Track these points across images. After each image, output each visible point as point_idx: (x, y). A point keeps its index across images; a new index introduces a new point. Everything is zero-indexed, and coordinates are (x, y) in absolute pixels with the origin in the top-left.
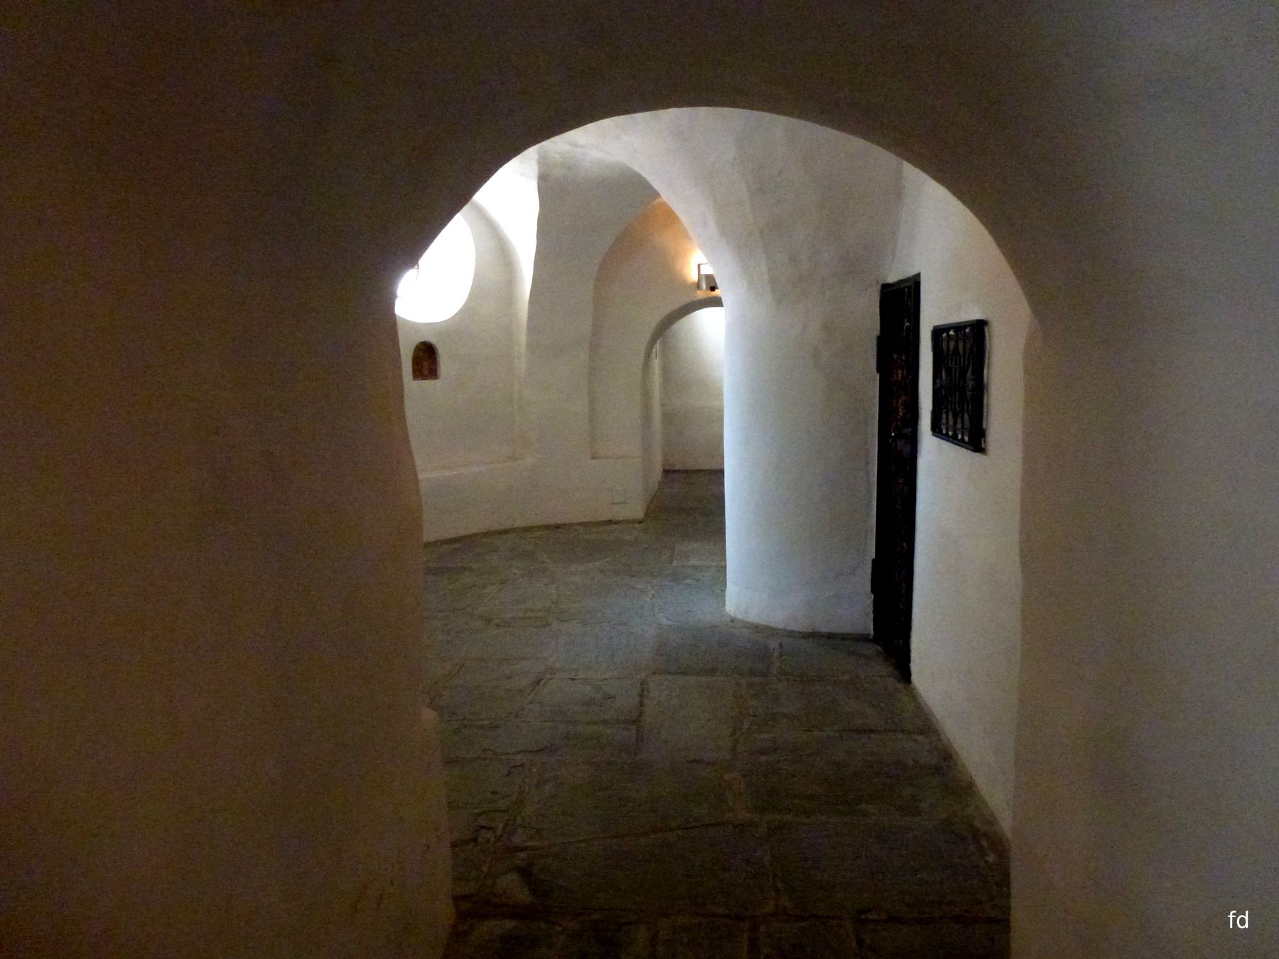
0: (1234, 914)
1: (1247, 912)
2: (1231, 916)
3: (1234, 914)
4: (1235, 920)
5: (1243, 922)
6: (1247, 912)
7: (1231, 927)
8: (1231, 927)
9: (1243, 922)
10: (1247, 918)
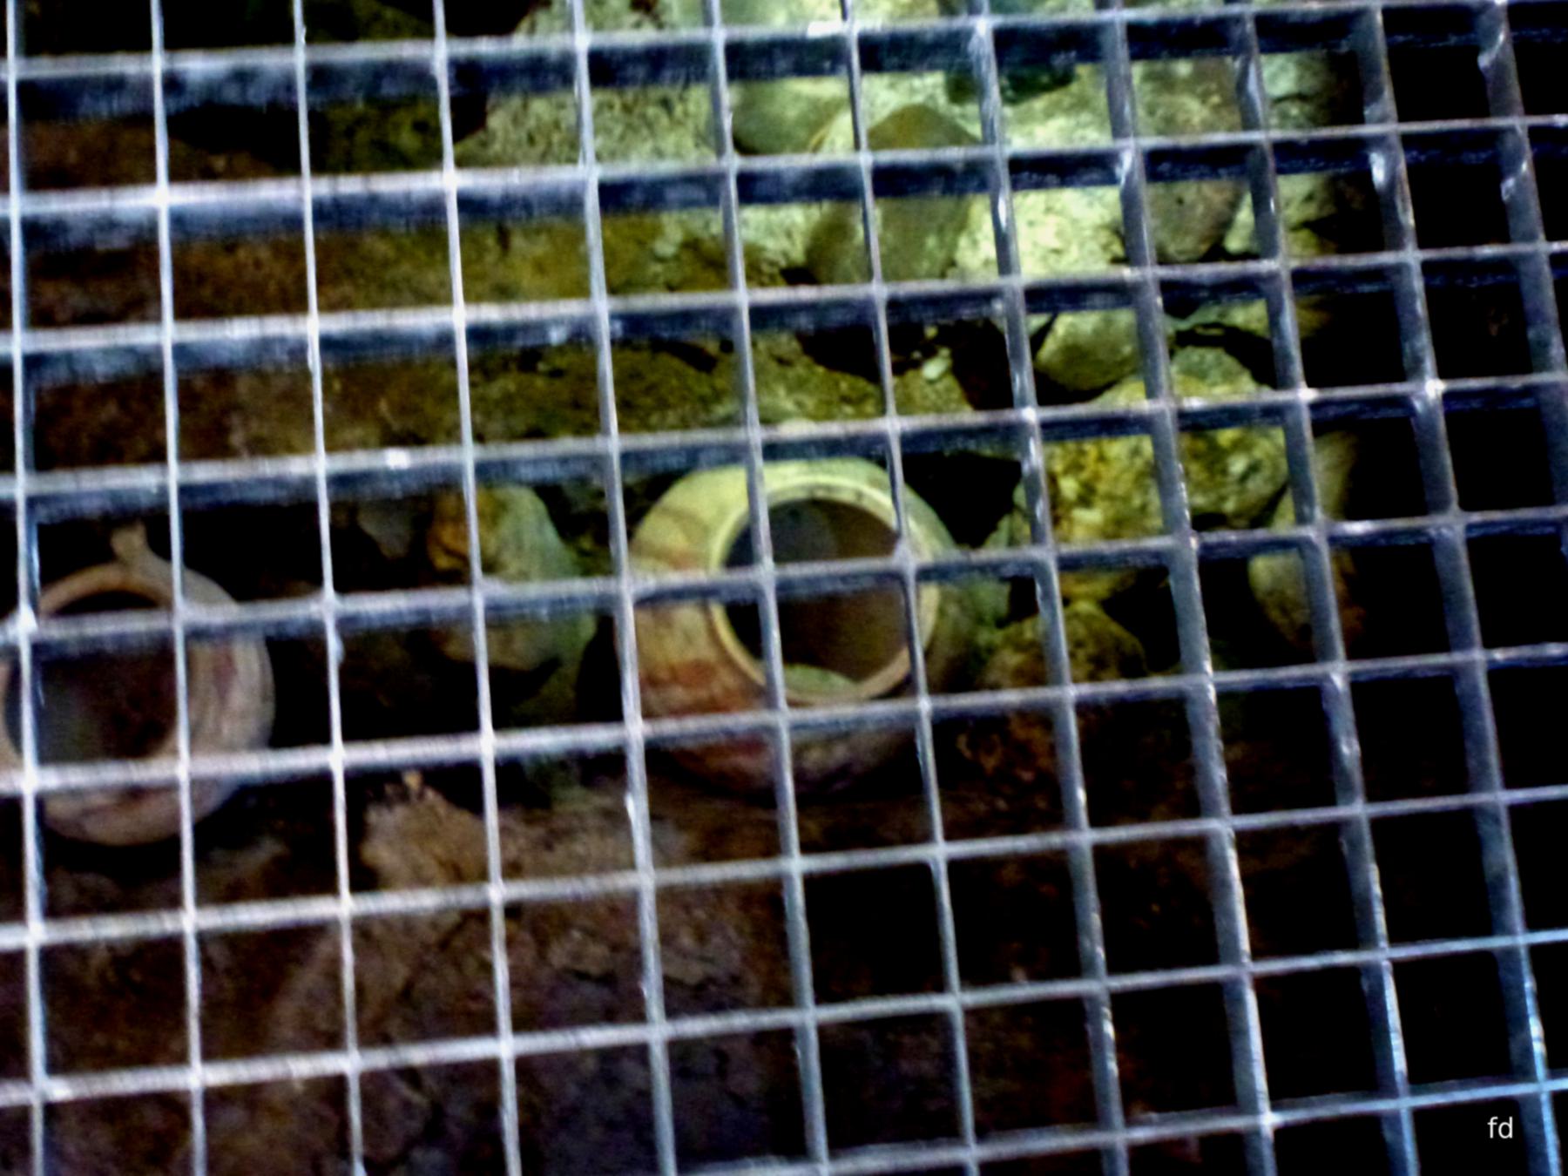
0: (1495, 1121)
1: (1511, 1119)
2: (1491, 1124)
3: (1495, 1121)
4: (1496, 1128)
5: (1505, 1130)
6: (1511, 1119)
7: (1492, 1136)
8: (1492, 1136)
9: (1505, 1130)
10: (1510, 1126)
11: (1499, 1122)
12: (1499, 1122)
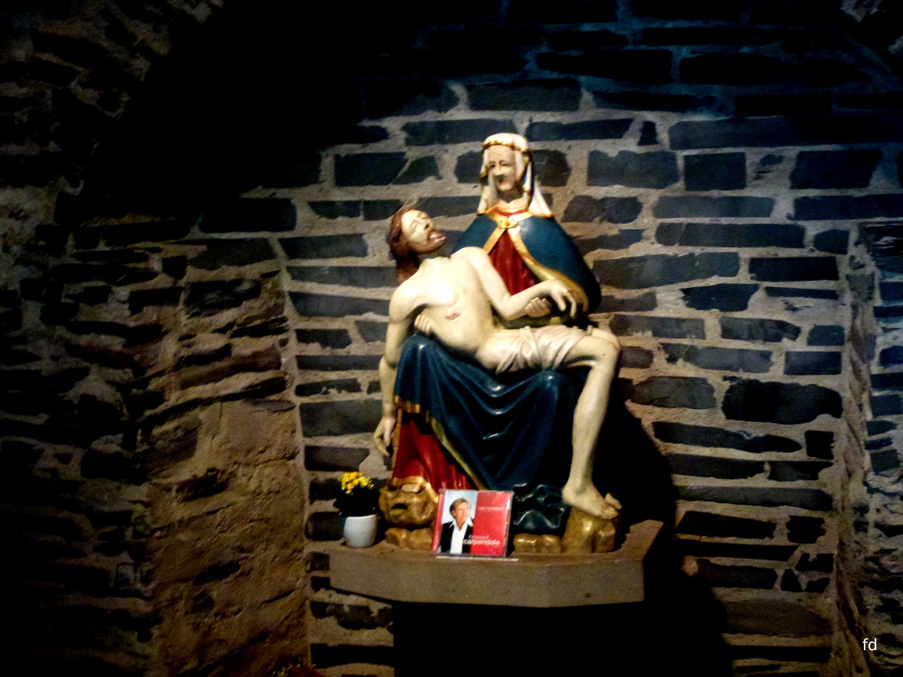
0: (866, 641)
1: (876, 639)
3: (866, 641)
4: (867, 645)
5: (872, 646)
6: (876, 639)
9: (872, 646)
10: (875, 643)
11: (868, 641)
12: (868, 641)
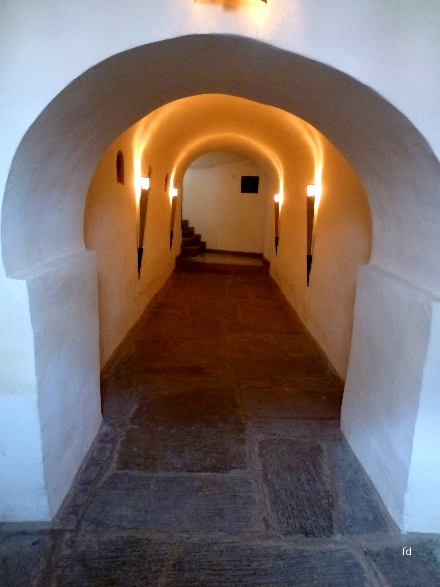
0: (405, 549)
1: (411, 548)
2: (403, 550)
3: (405, 549)
4: (405, 552)
6: (411, 548)
7: (404, 555)
8: (404, 555)
11: (406, 549)
12: (406, 549)
